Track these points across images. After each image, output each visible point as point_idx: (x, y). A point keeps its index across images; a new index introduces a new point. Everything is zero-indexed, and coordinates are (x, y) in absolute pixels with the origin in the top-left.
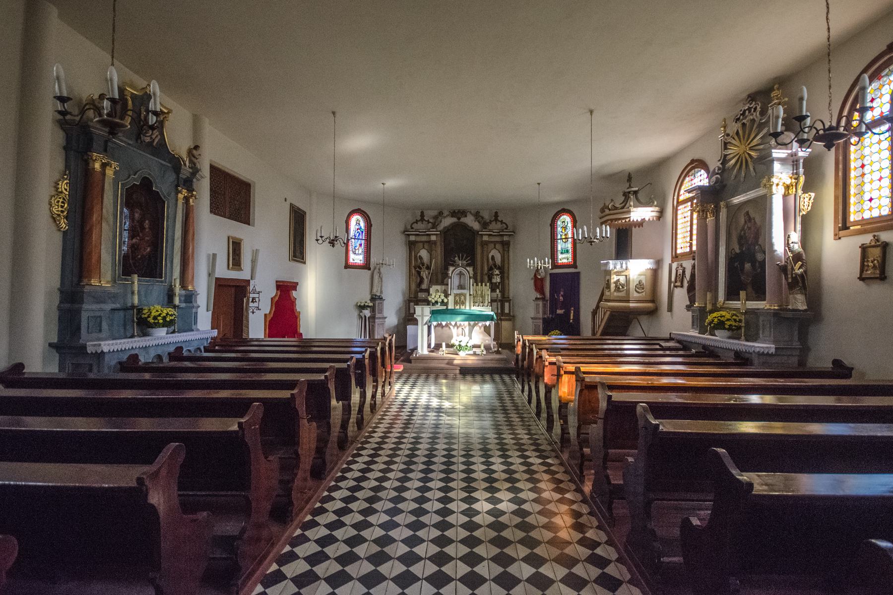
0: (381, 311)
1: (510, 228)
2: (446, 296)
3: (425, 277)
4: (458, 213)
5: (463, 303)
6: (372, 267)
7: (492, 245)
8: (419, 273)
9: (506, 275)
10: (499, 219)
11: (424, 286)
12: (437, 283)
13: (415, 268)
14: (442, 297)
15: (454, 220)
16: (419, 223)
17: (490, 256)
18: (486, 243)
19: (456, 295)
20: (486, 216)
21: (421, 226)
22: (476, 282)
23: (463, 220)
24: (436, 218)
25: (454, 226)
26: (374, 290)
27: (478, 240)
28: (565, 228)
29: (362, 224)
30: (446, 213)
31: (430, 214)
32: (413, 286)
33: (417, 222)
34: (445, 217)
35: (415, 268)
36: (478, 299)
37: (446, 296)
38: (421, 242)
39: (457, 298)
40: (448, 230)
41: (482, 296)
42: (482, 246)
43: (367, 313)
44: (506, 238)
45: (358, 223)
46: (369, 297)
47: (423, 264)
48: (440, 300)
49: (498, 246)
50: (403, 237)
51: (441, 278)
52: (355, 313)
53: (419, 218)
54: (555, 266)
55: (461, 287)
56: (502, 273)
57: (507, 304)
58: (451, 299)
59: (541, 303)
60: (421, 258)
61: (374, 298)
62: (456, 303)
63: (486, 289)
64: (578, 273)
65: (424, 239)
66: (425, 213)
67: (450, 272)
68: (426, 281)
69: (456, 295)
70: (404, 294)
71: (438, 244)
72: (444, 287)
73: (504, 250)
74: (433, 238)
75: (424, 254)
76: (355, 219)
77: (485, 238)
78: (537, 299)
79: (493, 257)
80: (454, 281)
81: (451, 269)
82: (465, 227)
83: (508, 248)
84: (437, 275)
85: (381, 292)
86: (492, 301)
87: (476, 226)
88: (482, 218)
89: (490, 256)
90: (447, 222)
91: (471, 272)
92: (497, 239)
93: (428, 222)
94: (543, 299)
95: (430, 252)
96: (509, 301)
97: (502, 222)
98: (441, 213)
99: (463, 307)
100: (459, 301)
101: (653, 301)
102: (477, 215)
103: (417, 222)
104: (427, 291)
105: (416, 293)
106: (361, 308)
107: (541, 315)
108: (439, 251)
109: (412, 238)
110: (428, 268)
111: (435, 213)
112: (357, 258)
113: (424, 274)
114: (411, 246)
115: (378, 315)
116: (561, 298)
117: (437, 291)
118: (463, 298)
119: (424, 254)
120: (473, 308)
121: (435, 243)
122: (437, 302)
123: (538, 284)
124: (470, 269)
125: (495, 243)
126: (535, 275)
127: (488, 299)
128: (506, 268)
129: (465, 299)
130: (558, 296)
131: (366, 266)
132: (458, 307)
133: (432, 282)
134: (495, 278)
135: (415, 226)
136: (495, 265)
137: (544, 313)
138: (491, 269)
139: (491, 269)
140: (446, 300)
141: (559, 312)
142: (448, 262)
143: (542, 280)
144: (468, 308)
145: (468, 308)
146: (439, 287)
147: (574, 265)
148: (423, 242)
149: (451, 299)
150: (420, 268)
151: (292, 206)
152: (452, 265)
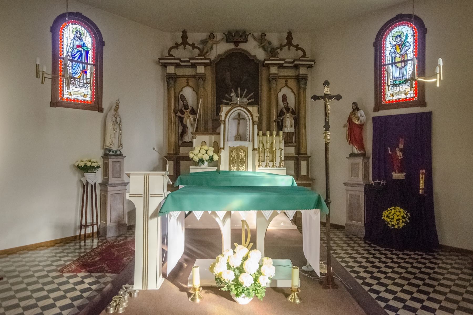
0: (119, 173)
1: (308, 55)
2: (218, 150)
3: (188, 125)
4: (236, 37)
5: (243, 162)
6: (105, 106)
7: (283, 81)
8: (181, 120)
9: (302, 122)
10: (294, 42)
11: (187, 138)
12: (206, 132)
13: (178, 112)
14: (211, 153)
15: (231, 46)
16: (181, 47)
17: (280, 95)
18: (276, 77)
19: (232, 150)
20: (274, 39)
21: (180, 53)
22: (260, 129)
23: (242, 46)
24: (204, 42)
25: (229, 55)
26: (108, 143)
27: (264, 74)
28: (402, 45)
29: (88, 40)
30: (219, 36)
31: (196, 37)
32: (173, 138)
33: (176, 46)
34: (217, 43)
35: (176, 113)
36: (266, 156)
37: (218, 150)
38: (183, 76)
39: (234, 154)
40: (221, 60)
41: (272, 151)
42: (269, 81)
43: (95, 178)
44: (302, 71)
45: (78, 36)
46: (101, 153)
47: (186, 107)
48: (206, 157)
49: (292, 83)
50: (159, 69)
51: (212, 125)
52: (74, 179)
53: (180, 41)
54: (379, 104)
55: (240, 137)
56: (297, 121)
57: (304, 164)
58: (224, 155)
59: (360, 161)
60: (183, 98)
61: (108, 154)
62: (232, 161)
63: (278, 142)
64: (429, 115)
65: (188, 71)
66: (189, 34)
67: (223, 114)
68: (190, 129)
69: (232, 150)
70: (160, 151)
71: (209, 77)
72: (213, 138)
73: (299, 88)
74: (201, 70)
75: (188, 93)
76: (70, 31)
77: (274, 70)
78: (352, 155)
79: (284, 98)
80: (230, 127)
81: (225, 109)
82: (246, 58)
83: (306, 84)
84: (206, 122)
85: (120, 145)
86: (287, 158)
87: (260, 54)
88: (270, 43)
89: (280, 95)
90: (221, 48)
91: (256, 115)
92: (291, 73)
93: (193, 46)
94: (364, 155)
95: (196, 91)
96: (307, 158)
97: (297, 48)
98: (212, 36)
99: (242, 168)
100: (238, 158)
101: (175, 154)
102: (262, 40)
103: (176, 46)
104: (190, 144)
105: (177, 147)
106: (85, 169)
107: (360, 179)
108: (209, 88)
109: (171, 70)
110: (193, 112)
111: (204, 36)
112: (80, 92)
113: (189, 120)
114: (171, 80)
115: (112, 180)
116: (399, 154)
117: (204, 143)
118: (242, 154)
119: (188, 93)
120: (258, 169)
121: (202, 77)
122: (201, 161)
123: (354, 133)
124: (254, 110)
125: (286, 78)
126: (350, 120)
127: (280, 155)
128: (302, 113)
129: (246, 155)
130: (394, 151)
131: (96, 106)
132: (235, 168)
133: (197, 131)
134: (286, 125)
135: (175, 53)
136: (288, 109)
137: (366, 176)
138: (281, 114)
139: (281, 114)
140: (216, 158)
141: (397, 175)
142: (222, 97)
143: (361, 127)
144: (250, 169)
145: (250, 169)
146: (206, 138)
147: (422, 102)
148: (188, 77)
149: (224, 155)
150: (183, 113)
151: (319, 195)
152: (227, 104)
